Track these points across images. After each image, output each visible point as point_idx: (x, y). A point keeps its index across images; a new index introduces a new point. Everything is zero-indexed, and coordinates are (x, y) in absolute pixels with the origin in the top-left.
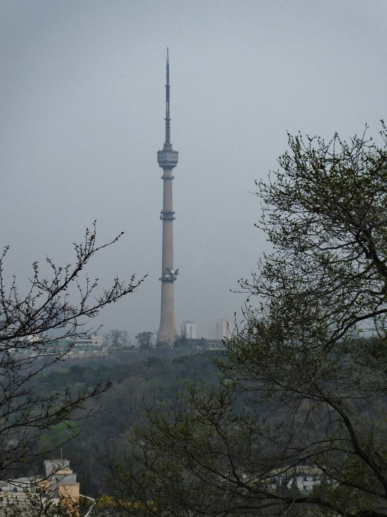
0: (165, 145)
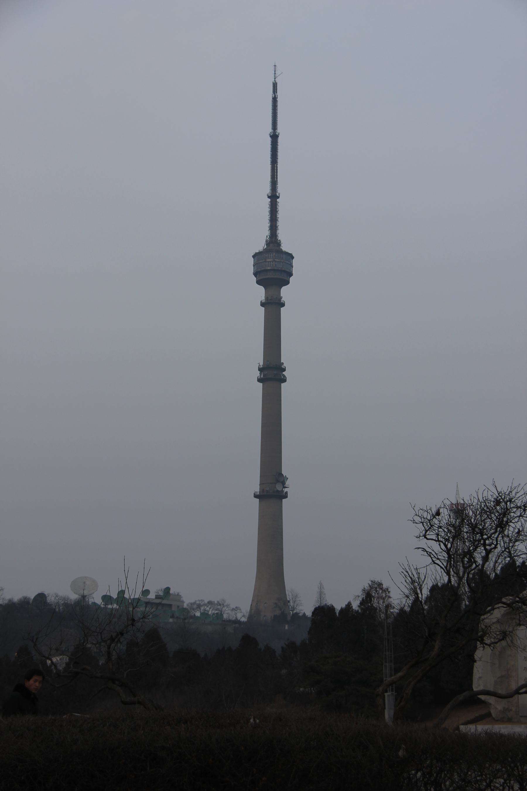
0: (268, 243)
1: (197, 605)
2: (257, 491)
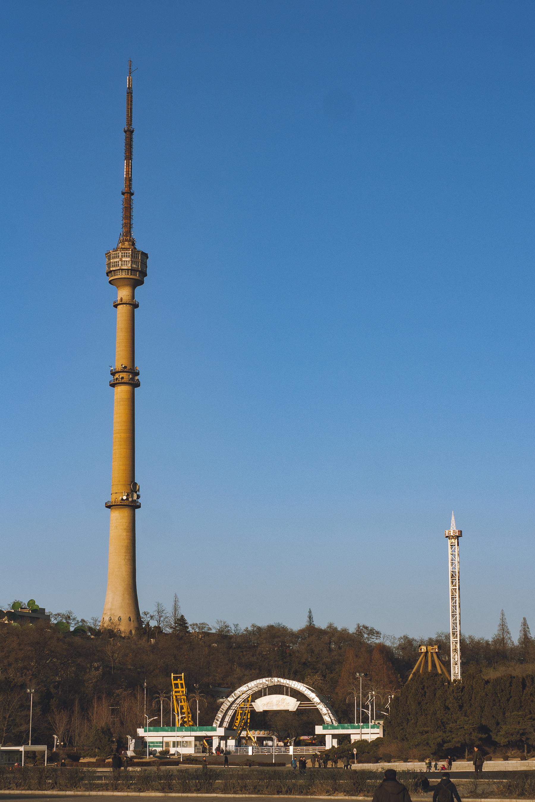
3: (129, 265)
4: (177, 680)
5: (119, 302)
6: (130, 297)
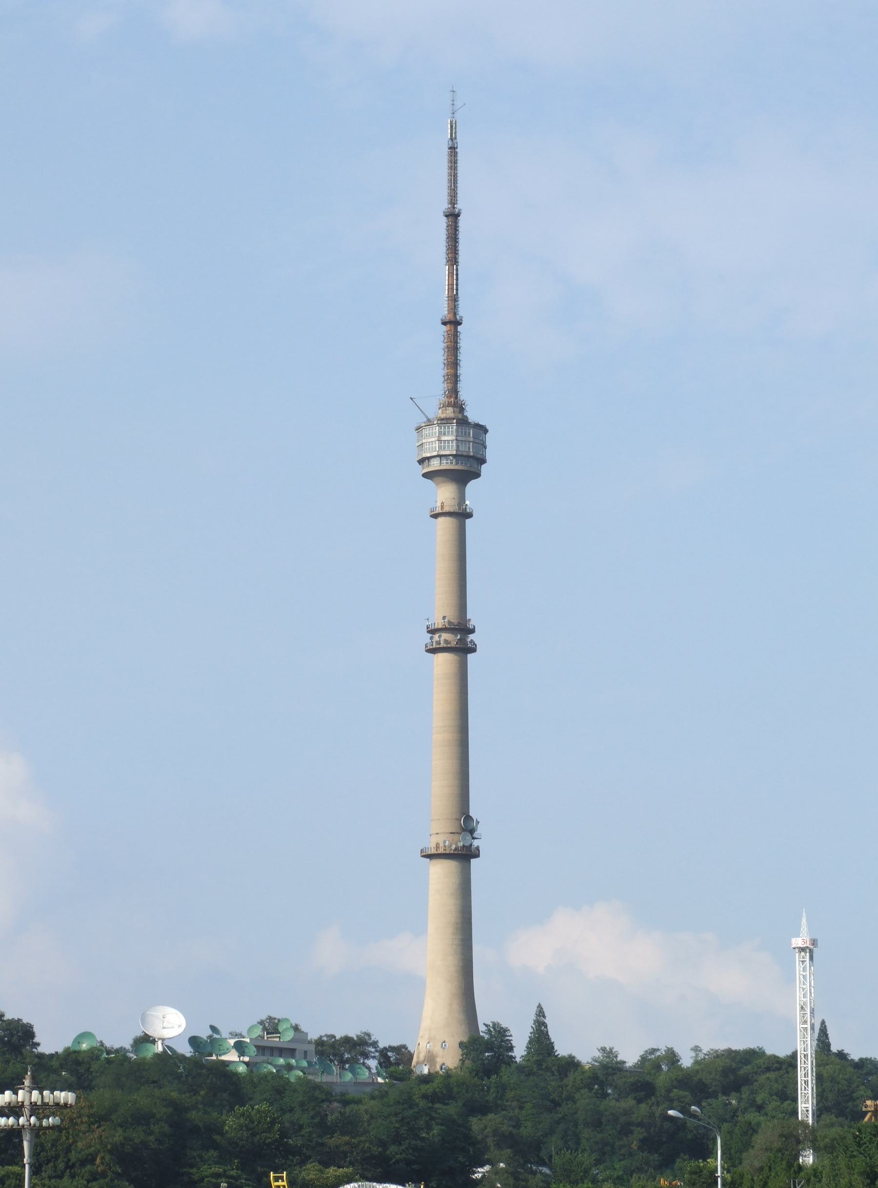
1: (708, 1171)
2: (427, 847)
3: (455, 447)
4: (279, 1182)
5: (438, 510)
6: (456, 502)
